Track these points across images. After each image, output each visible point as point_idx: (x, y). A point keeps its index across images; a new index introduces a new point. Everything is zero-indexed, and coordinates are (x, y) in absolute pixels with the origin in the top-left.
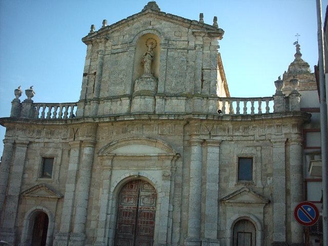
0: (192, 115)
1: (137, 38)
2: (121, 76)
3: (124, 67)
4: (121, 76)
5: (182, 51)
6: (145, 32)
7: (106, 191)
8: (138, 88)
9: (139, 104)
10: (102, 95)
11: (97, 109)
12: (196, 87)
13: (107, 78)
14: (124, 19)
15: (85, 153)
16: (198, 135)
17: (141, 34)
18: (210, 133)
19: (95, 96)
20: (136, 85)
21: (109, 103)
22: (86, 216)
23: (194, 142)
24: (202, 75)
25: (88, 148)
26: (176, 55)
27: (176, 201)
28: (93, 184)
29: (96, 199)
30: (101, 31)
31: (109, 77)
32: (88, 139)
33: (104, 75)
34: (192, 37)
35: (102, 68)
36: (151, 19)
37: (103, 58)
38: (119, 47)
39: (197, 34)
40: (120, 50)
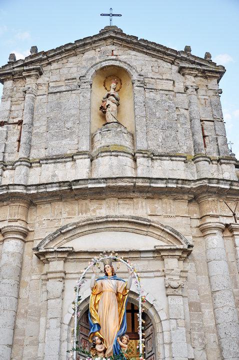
0: (206, 181)
1: (93, 71)
2: (69, 125)
3: (73, 112)
4: (69, 125)
5: (167, 93)
6: (104, 64)
7: (54, 323)
8: (101, 142)
9: (107, 167)
10: (35, 154)
11: (27, 175)
12: (195, 144)
13: (44, 128)
14: (70, 44)
15: (6, 250)
16: (217, 217)
17: (99, 66)
18: (234, 215)
19: (22, 154)
20: (96, 139)
21: (51, 166)
22: (11, 346)
23: (210, 228)
24: (203, 130)
25: (13, 242)
26: (158, 98)
27: (196, 337)
28: (23, 311)
29: (32, 343)
30: (30, 60)
31: (48, 127)
32: (106, 303)
33: (36, 124)
34: (178, 78)
35: (33, 114)
36: (113, 48)
37: (33, 99)
38: (62, 84)
39: (187, 71)
40: (63, 89)
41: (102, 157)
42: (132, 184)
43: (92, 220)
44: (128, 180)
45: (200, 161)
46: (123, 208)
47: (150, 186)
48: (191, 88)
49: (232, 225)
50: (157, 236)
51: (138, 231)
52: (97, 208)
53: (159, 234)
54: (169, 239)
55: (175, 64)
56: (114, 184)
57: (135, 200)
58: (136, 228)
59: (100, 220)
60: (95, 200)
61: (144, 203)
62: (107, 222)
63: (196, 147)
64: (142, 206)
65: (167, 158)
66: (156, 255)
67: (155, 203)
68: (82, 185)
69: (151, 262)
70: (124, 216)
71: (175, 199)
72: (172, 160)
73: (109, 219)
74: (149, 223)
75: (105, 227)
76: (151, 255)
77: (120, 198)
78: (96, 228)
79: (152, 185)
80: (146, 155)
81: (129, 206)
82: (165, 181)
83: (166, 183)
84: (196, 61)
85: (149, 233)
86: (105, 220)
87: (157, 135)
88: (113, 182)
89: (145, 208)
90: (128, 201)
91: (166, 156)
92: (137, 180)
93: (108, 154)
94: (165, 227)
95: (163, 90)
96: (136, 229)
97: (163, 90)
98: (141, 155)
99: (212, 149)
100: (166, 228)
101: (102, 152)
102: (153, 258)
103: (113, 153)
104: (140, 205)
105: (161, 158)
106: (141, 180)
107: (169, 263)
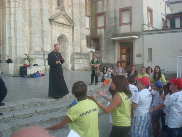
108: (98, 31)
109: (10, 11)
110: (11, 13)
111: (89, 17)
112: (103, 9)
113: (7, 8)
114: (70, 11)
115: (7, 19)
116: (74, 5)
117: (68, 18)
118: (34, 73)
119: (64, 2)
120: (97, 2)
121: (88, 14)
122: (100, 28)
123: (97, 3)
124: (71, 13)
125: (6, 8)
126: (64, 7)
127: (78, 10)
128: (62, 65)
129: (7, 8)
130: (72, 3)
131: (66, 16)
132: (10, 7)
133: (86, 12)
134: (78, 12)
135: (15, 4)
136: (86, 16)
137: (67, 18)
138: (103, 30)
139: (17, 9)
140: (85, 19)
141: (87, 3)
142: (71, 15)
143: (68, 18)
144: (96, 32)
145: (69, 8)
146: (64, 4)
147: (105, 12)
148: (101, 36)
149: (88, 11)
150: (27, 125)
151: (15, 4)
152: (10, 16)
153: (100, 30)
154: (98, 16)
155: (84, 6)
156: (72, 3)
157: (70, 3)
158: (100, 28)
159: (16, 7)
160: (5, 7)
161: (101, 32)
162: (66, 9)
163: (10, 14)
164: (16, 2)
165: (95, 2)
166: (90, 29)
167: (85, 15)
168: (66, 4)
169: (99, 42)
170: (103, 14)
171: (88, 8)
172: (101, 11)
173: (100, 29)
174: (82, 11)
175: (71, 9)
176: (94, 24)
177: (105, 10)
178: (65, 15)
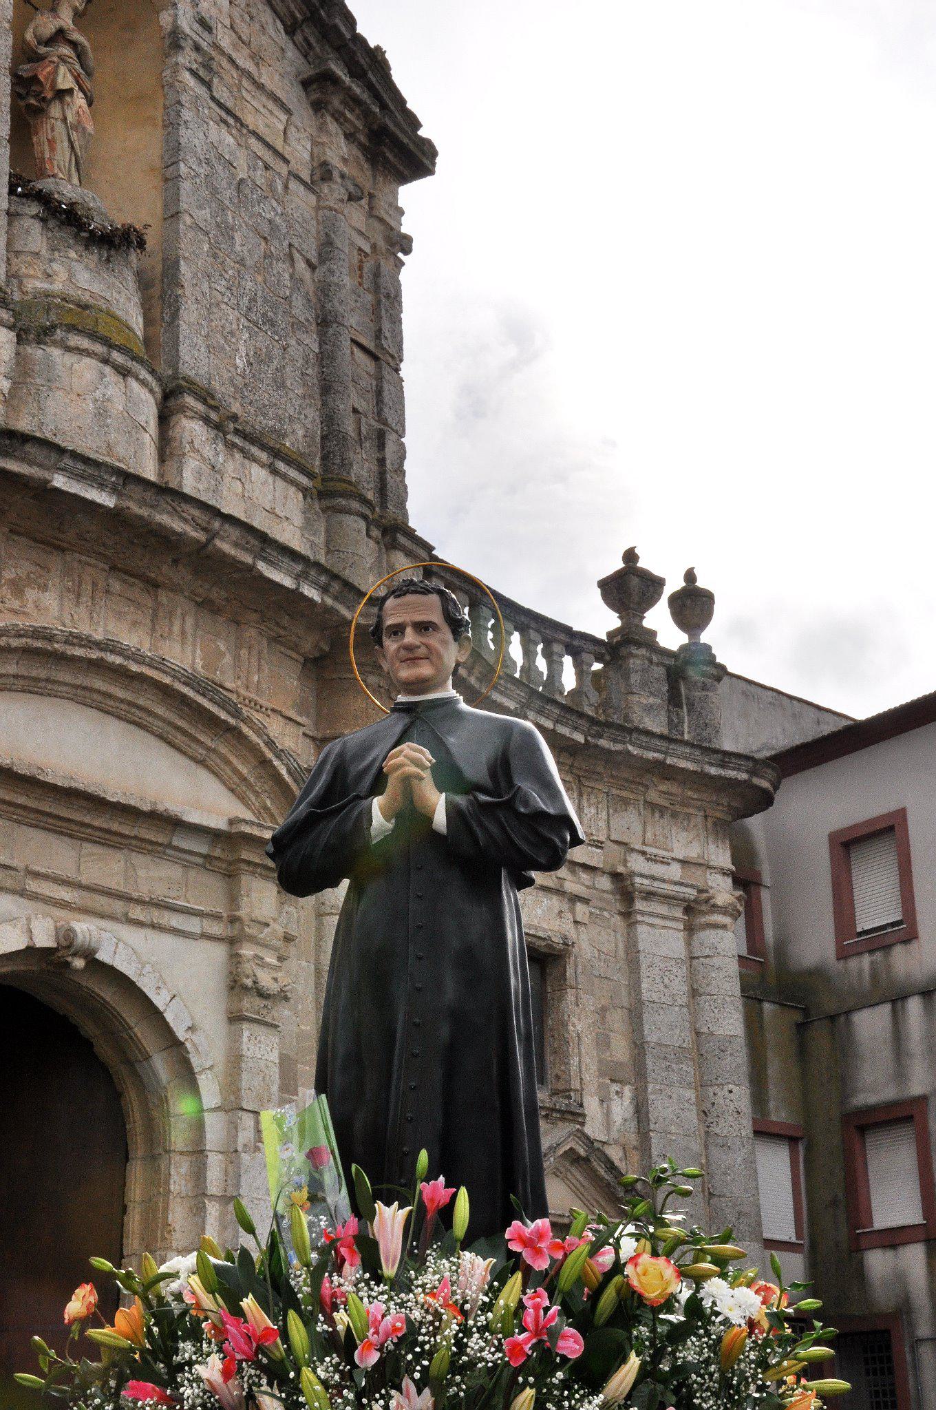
41: (68, 349)
42: (201, 536)
43: (50, 638)
44: (196, 513)
45: (349, 512)
46: (119, 615)
47: (251, 568)
48: (339, 180)
49: (638, 880)
50: (235, 779)
51: (179, 739)
52: (30, 581)
53: (244, 770)
54: (268, 802)
55: (299, 38)
56: (143, 512)
57: (163, 597)
58: (181, 723)
59: (79, 652)
60: (23, 539)
61: (190, 621)
62: (98, 666)
63: (332, 445)
64: (183, 632)
65: (264, 456)
66: (218, 853)
67: (218, 635)
68: (31, 463)
69: (192, 874)
70: (159, 664)
71: (275, 640)
72: (274, 472)
73: (112, 658)
74: (232, 721)
75: (78, 682)
76: (200, 846)
77: (120, 570)
78: (43, 674)
79: (262, 566)
80: (214, 416)
81: (139, 617)
82: (299, 568)
83: (297, 577)
84: (370, 75)
85: (213, 760)
86: (95, 655)
87: (232, 333)
88: (142, 503)
89: (190, 639)
90: (137, 593)
91: (263, 447)
92: (227, 526)
93: (99, 348)
94: (279, 754)
95: (260, 138)
96: (177, 728)
97: (260, 138)
98: (200, 407)
99: (364, 473)
100: (279, 757)
101: (72, 328)
102: (200, 860)
103: (117, 356)
104: (176, 628)
105: (247, 446)
106: (235, 533)
107: (253, 895)
108: (878, 1262)
109: (199, 1174)
110: (205, 1195)
111: (792, 1141)
112: (900, 1074)
113: (182, 1153)
114: (621, 1109)
115: (177, 1235)
116: (649, 1061)
117: (608, 1177)
118: (403, 473)
119: (572, 1049)
120: (848, 1013)
121: (779, 1114)
122: (894, 1238)
123: (849, 1023)
124: (632, 1125)
125: (176, 1158)
126: (575, 1084)
127: (690, 1094)
128: (705, 637)
129: (182, 1153)
130: (639, 1047)
131: (587, 1160)
132: (202, 1151)
133: (759, 1099)
134: (692, 1116)
135: (234, 1127)
136: (759, 1133)
137: (594, 1176)
138: (914, 1258)
139: (245, 1157)
140: (751, 1162)
141: (761, 1022)
142: (633, 1139)
143: (608, 1177)
144: (860, 1274)
145: (615, 1087)
146: (574, 1061)
147: (923, 1100)
148: (904, 1310)
149: (773, 1091)
150: (361, 277)
151: (234, 1127)
152: (199, 1211)
153: (890, 1254)
154: (863, 1130)
155: (737, 1059)
156: (639, 1047)
157: (620, 1050)
158: (894, 1238)
159: (240, 1149)
160: (168, 1152)
161: (900, 1277)
162: (592, 1106)
163: (199, 1196)
164: (240, 1113)
165: (833, 1018)
166: (805, 1242)
167: (747, 1131)
168: (586, 1059)
169: (891, 1371)
170: (909, 1119)
171: (774, 1069)
172: (888, 1093)
173: (894, 1246)
174: (719, 1100)
175: (628, 1091)
176: (834, 1203)
177: (916, 1088)
178: (582, 1152)
